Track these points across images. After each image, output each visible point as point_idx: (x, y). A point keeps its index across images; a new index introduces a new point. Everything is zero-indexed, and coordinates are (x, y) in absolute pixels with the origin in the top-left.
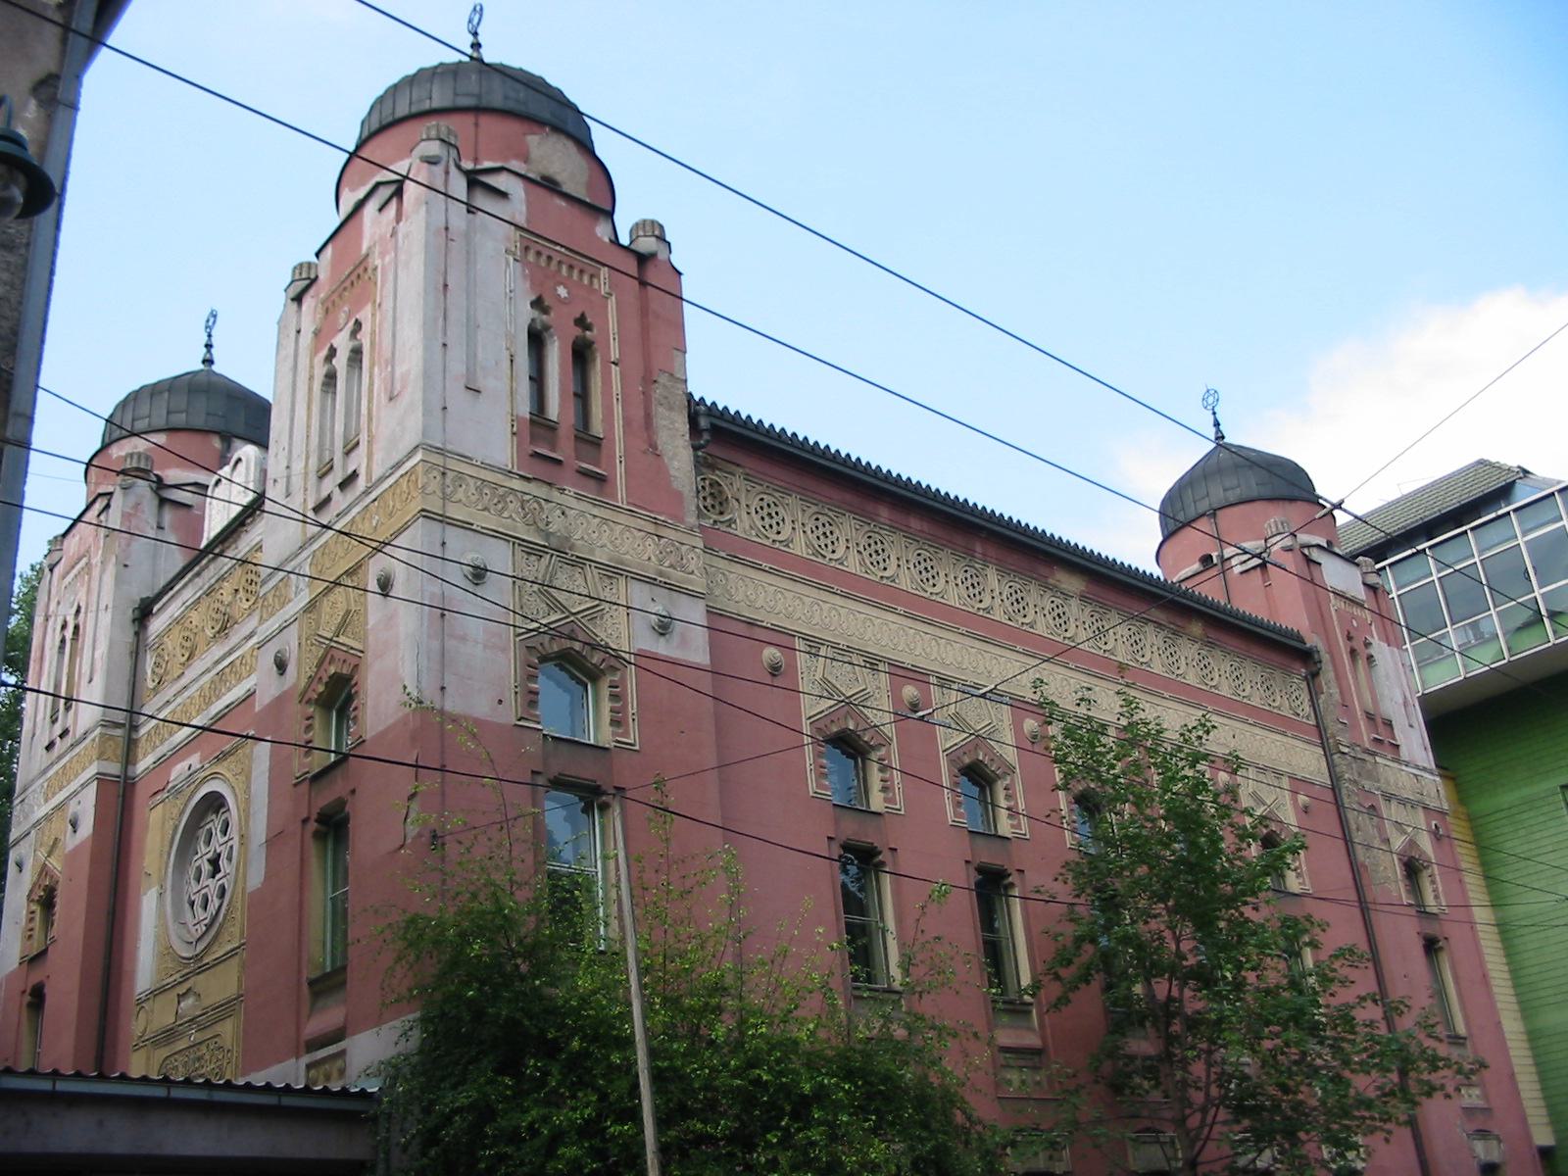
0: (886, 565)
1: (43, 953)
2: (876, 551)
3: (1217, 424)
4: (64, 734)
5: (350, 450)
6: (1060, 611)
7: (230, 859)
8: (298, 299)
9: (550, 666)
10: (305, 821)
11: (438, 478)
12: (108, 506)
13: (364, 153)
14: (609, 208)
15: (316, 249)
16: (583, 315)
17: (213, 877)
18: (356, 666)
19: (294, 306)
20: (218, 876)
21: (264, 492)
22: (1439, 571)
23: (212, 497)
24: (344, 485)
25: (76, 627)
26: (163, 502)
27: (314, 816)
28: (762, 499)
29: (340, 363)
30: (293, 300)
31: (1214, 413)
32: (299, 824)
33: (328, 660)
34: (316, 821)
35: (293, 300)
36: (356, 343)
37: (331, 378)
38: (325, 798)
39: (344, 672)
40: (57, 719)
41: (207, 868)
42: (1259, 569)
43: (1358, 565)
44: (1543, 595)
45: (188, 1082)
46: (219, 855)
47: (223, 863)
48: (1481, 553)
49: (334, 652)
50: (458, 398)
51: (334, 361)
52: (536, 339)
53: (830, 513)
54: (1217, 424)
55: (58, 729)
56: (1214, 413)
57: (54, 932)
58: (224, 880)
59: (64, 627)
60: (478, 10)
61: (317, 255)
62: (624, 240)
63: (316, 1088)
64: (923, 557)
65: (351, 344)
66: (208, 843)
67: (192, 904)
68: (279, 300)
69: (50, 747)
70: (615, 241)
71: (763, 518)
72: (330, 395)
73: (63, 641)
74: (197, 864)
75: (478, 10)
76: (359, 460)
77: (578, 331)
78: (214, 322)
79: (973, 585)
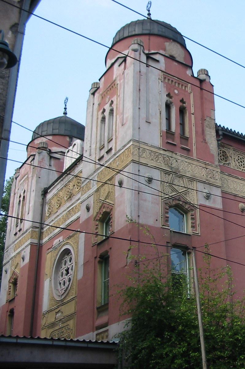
1: (14, 299)
4: (20, 230)
5: (110, 141)
7: (72, 269)
9: (172, 209)
10: (96, 258)
11: (137, 150)
12: (34, 159)
14: (191, 65)
15: (99, 78)
16: (183, 99)
17: (67, 275)
18: (112, 209)
19: (92, 96)
20: (68, 275)
21: (83, 154)
23: (66, 156)
25: (24, 197)
26: (51, 157)
28: (239, 157)
30: (92, 94)
34: (99, 258)
35: (92, 94)
36: (112, 108)
37: (104, 119)
39: (108, 211)
40: (18, 226)
41: (65, 272)
46: (69, 268)
47: (70, 271)
49: (104, 204)
50: (144, 125)
51: (105, 113)
55: (18, 229)
57: (17, 293)
58: (70, 276)
59: (20, 197)
61: (99, 80)
62: (196, 75)
65: (110, 108)
66: (65, 264)
67: (60, 284)
68: (87, 94)
69: (16, 234)
70: (193, 76)
72: (103, 124)
73: (20, 201)
74: (62, 271)
76: (112, 144)
77: (181, 104)
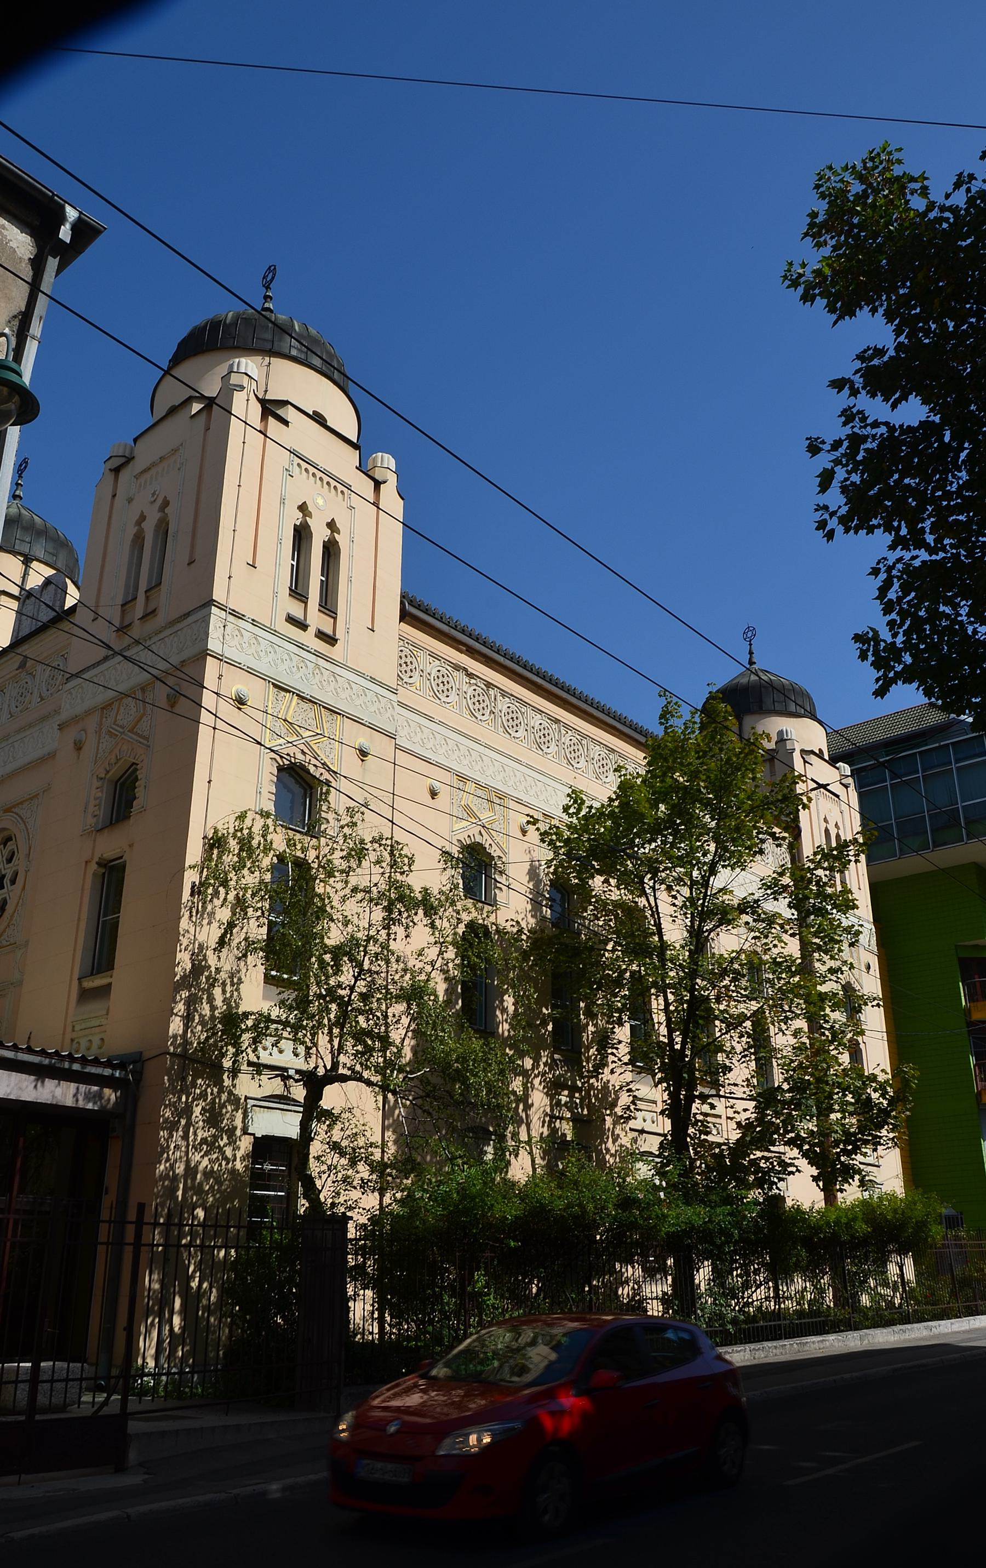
0: (607, 774)
2: (512, 718)
3: (751, 653)
6: (481, 699)
8: (117, 471)
13: (177, 372)
19: (111, 477)
22: (891, 780)
24: (149, 614)
27: (96, 859)
29: (149, 527)
31: (750, 645)
32: (84, 863)
33: (732, 1095)
34: (97, 863)
38: (109, 846)
42: (768, 763)
43: (838, 769)
44: (963, 807)
45: (71, 1058)
48: (923, 772)
52: (301, 535)
53: (517, 704)
54: (751, 653)
56: (750, 645)
60: (272, 270)
61: (135, 440)
63: (50, 1051)
64: (543, 726)
71: (474, 704)
75: (272, 270)
78: (25, 467)
79: (544, 735)
